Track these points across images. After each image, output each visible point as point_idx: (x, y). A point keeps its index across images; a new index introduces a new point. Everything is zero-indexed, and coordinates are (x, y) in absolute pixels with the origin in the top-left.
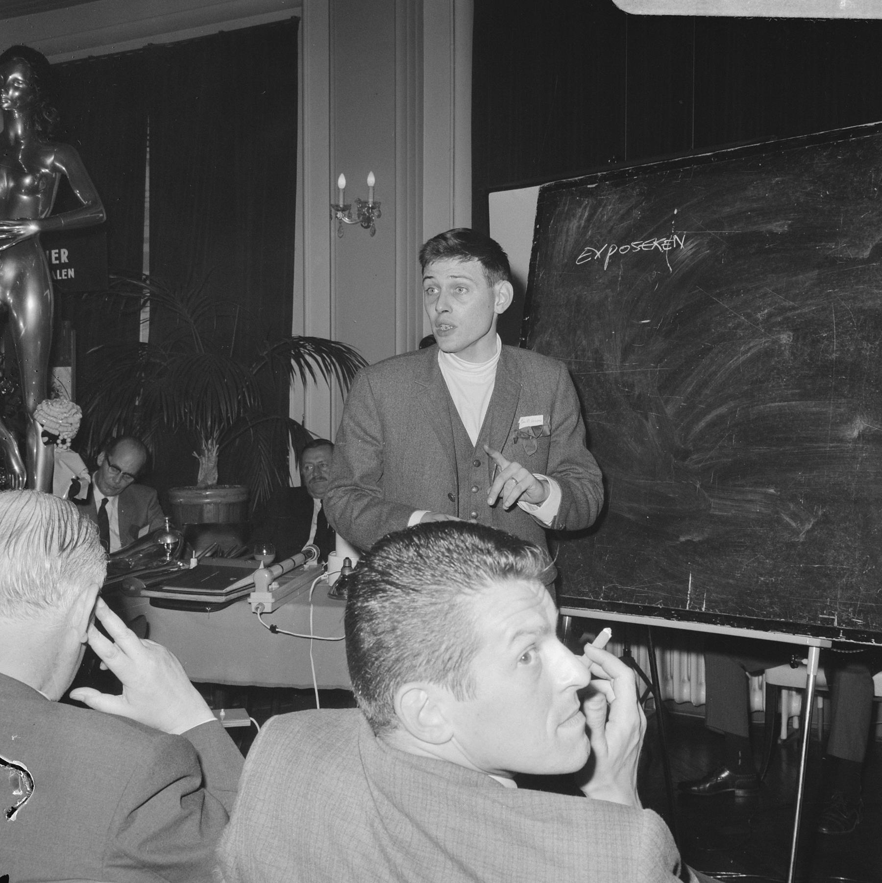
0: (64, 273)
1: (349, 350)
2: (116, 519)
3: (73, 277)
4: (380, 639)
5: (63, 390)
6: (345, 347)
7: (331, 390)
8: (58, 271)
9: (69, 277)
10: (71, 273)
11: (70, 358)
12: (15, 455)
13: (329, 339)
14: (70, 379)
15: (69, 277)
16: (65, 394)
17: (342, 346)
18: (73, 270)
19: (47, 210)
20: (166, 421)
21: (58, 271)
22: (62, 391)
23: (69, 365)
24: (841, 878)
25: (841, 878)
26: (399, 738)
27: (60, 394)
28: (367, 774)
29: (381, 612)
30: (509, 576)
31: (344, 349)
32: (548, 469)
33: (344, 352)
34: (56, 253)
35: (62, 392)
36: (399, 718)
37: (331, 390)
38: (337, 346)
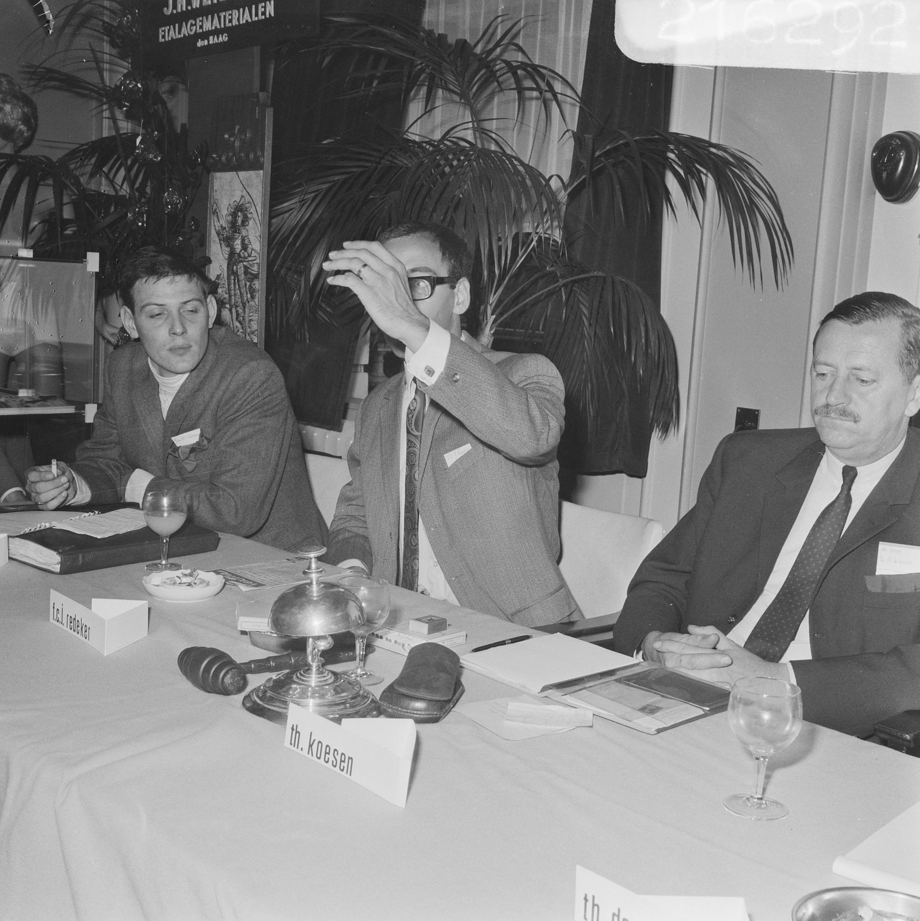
0: (261, 10)
1: (741, 163)
2: (333, 279)
3: (273, 15)
4: (442, 63)
5: (253, 210)
6: (733, 156)
7: (702, 228)
8: (254, 6)
11: (263, 155)
13: (708, 139)
15: (268, 16)
16: (255, 215)
17: (726, 151)
21: (254, 6)
22: (252, 210)
26: (338, 629)
27: (249, 216)
28: (498, 50)
30: (445, 263)
31: (731, 159)
33: (732, 164)
36: (369, 541)
38: (720, 153)
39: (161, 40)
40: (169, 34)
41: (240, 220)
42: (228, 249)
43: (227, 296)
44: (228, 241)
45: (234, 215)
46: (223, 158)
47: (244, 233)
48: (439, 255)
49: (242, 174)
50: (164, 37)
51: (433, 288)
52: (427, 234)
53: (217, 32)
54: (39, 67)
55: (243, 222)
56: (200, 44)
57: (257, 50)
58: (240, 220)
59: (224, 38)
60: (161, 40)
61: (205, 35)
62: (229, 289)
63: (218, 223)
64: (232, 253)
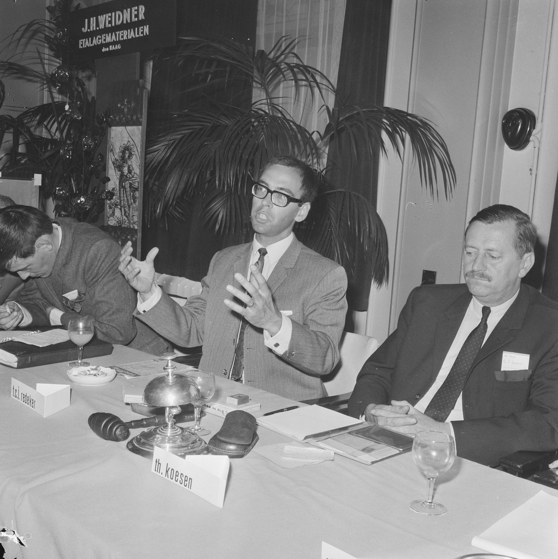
0: (141, 31)
3: (148, 34)
5: (135, 149)
6: (421, 121)
7: (403, 163)
8: (136, 29)
9: (145, 34)
10: (146, 29)
11: (142, 117)
12: (218, 223)
14: (140, 136)
15: (145, 34)
16: (136, 153)
18: (148, 26)
19: (433, 151)
20: (217, 184)
23: (137, 123)
24: (528, 129)
25: (528, 129)
27: (133, 153)
29: (366, 433)
31: (419, 123)
32: (255, 279)
34: (135, 11)
35: (134, 151)
37: (403, 163)
39: (80, 47)
40: (85, 43)
41: (127, 156)
42: (119, 173)
43: (119, 201)
44: (119, 167)
45: (123, 152)
46: (135, 117)
47: (129, 163)
48: (300, 184)
49: (129, 128)
50: (82, 45)
51: (288, 203)
52: (299, 170)
53: (114, 43)
54: (6, 62)
55: (129, 157)
56: (104, 50)
57: (138, 54)
58: (127, 156)
59: (118, 47)
60: (80, 47)
61: (107, 45)
62: (120, 197)
63: (112, 158)
64: (122, 175)
